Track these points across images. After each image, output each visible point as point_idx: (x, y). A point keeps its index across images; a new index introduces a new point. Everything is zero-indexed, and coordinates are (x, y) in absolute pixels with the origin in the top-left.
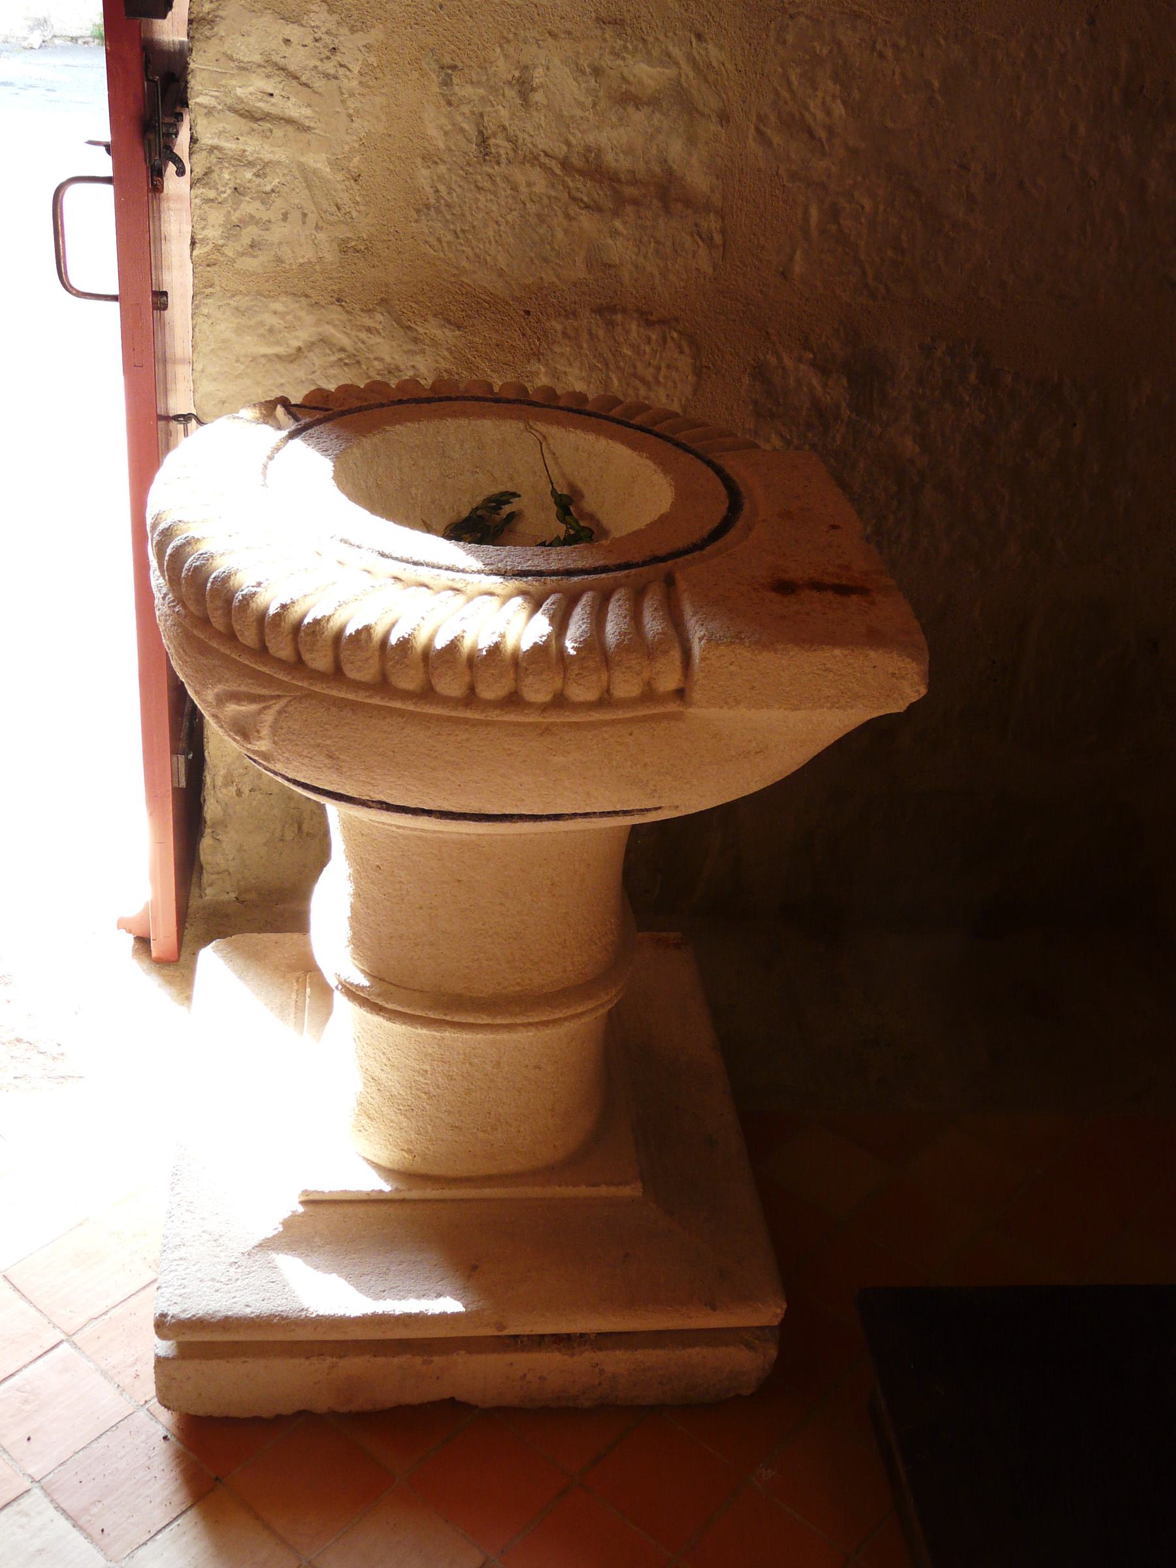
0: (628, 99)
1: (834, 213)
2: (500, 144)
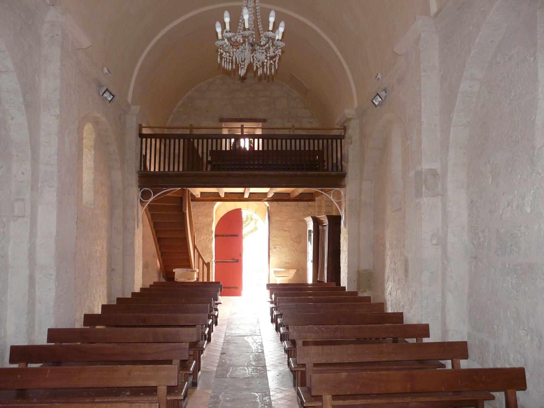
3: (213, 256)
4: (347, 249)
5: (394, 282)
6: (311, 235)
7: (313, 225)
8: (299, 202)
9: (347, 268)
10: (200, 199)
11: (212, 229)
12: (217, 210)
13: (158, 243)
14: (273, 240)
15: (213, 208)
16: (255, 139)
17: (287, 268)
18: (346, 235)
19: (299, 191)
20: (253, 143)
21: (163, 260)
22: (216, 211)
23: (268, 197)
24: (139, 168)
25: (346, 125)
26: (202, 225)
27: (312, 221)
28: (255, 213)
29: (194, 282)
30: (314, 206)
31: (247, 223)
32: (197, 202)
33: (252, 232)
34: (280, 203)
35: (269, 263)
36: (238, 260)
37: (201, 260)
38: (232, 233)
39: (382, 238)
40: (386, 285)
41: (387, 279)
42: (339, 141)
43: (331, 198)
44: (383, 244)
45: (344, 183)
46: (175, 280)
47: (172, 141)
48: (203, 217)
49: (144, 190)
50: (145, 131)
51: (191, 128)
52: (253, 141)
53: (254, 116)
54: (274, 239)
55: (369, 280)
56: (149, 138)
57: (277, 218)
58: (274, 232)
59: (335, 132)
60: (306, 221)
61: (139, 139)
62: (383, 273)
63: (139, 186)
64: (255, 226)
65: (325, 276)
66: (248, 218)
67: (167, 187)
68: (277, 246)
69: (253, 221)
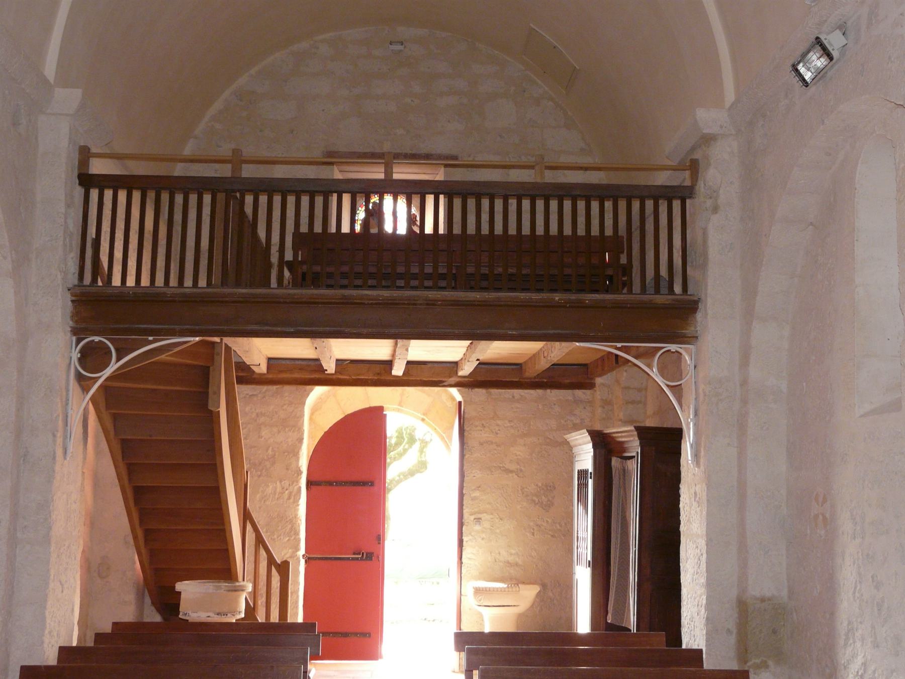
0: (511, 554)
1: (537, 566)
2: (497, 560)
3: (299, 540)
4: (704, 529)
5: (876, 645)
6: (586, 485)
7: (592, 454)
8: (549, 391)
9: (703, 590)
10: (267, 379)
11: (300, 464)
12: (313, 412)
13: (137, 501)
14: (473, 499)
15: (304, 404)
16: (427, 196)
17: (511, 579)
18: (698, 487)
19: (552, 355)
20: (418, 223)
21: (152, 554)
22: (312, 413)
23: (460, 373)
24: (77, 275)
25: (697, 155)
26: (270, 452)
27: (591, 445)
28: (423, 420)
29: (238, 624)
30: (591, 403)
31: (400, 449)
32: (258, 387)
33: (411, 473)
34: (495, 391)
35: (461, 563)
36: (373, 553)
37: (263, 553)
38: (356, 477)
39: (821, 499)
40: (844, 655)
41: (847, 635)
42: (676, 204)
43: (654, 373)
44: (825, 519)
45: (693, 329)
46: (180, 616)
47: (179, 199)
48: (275, 430)
49: (88, 343)
50: (98, 167)
51: (237, 159)
52: (418, 218)
53: (424, 147)
54: (476, 494)
55: (774, 632)
56: (109, 187)
57: (485, 435)
58: (475, 474)
59: (662, 179)
60: (572, 444)
61: (79, 191)
62: (832, 614)
63: (71, 331)
64: (420, 460)
65: (629, 610)
66: (403, 438)
67: (159, 333)
68: (485, 514)
69: (417, 446)
